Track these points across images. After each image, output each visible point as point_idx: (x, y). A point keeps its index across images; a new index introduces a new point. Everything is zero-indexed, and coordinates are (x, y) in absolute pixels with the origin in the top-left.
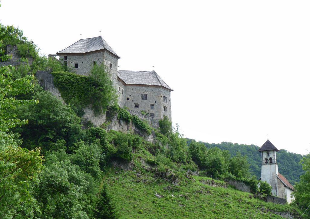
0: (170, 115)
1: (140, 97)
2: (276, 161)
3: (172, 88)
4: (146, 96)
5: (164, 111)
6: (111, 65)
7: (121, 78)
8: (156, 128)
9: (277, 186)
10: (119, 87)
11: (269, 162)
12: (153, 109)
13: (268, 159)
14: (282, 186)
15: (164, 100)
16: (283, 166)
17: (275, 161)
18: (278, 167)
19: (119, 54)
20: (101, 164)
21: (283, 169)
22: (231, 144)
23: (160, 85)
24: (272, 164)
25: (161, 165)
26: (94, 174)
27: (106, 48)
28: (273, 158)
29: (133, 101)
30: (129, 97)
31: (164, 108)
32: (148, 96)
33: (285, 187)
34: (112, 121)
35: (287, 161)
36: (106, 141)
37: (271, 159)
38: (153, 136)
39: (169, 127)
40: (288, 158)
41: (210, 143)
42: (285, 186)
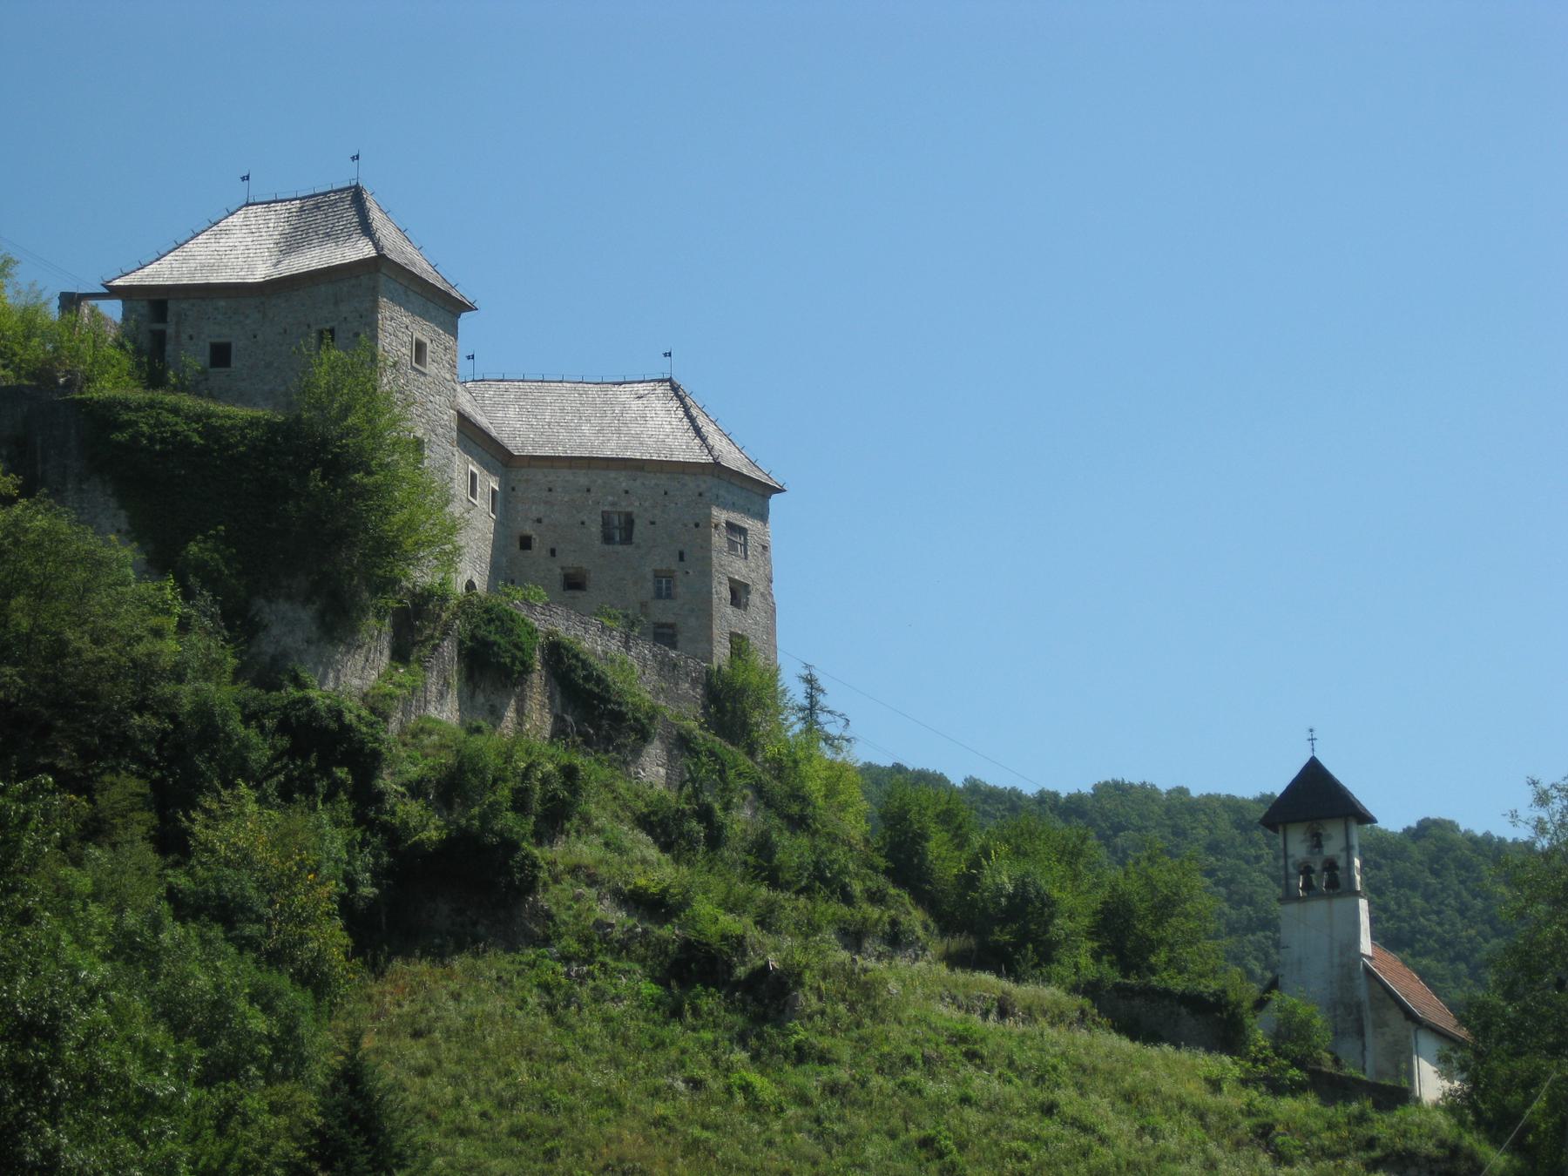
0: (771, 631)
1: (596, 529)
2: (1358, 878)
3: (776, 480)
4: (629, 521)
5: (729, 610)
6: (420, 348)
7: (482, 420)
8: (688, 714)
9: (1369, 1017)
10: (473, 476)
11: (1320, 881)
12: (669, 596)
13: (1318, 867)
14: (1395, 1018)
15: (732, 546)
16: (1438, 913)
17: (1351, 880)
18: (1370, 903)
19: (462, 292)
20: (1123, 977)
21: (1439, 930)
22: (1147, 794)
23: (705, 458)
24: (1339, 895)
25: (704, 907)
26: (315, 980)
27: (386, 252)
28: (1341, 863)
29: (553, 552)
30: (528, 530)
31: (733, 592)
32: (637, 521)
33: (1410, 1023)
34: (425, 669)
35: (1462, 882)
36: (387, 782)
37: (1331, 866)
38: (669, 752)
39: (759, 703)
40: (1465, 865)
41: (1029, 790)
42: (1409, 1015)
